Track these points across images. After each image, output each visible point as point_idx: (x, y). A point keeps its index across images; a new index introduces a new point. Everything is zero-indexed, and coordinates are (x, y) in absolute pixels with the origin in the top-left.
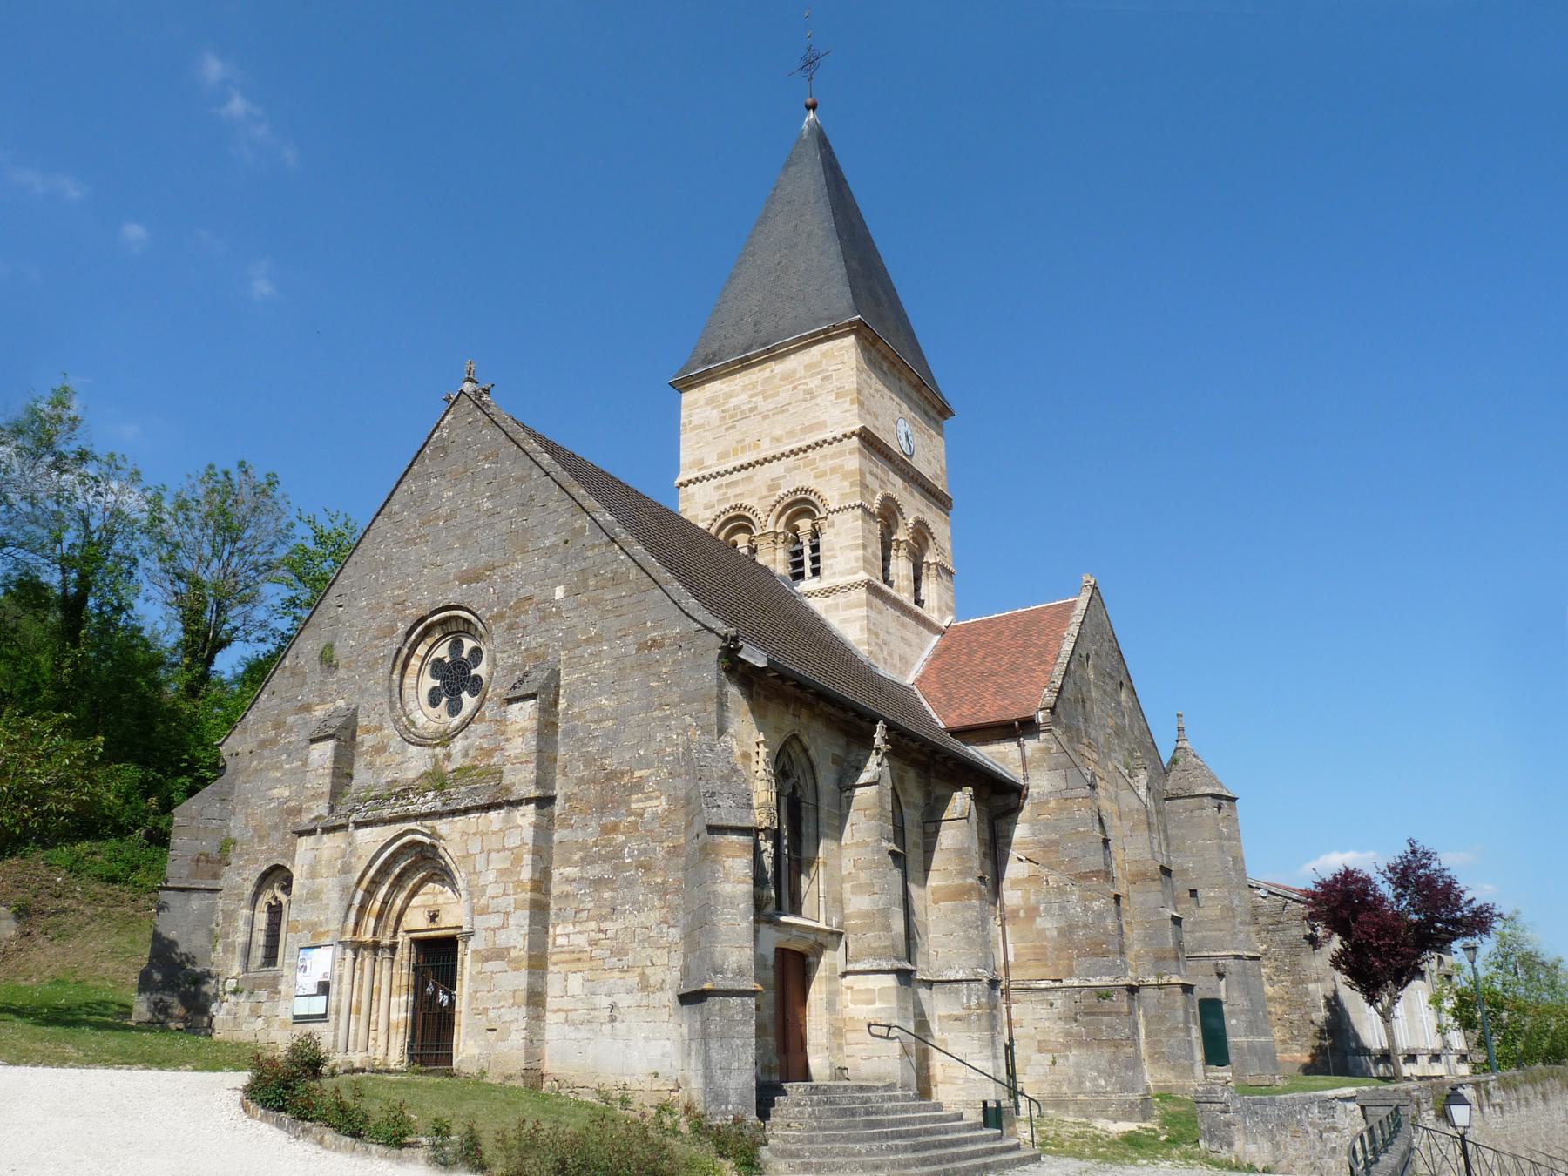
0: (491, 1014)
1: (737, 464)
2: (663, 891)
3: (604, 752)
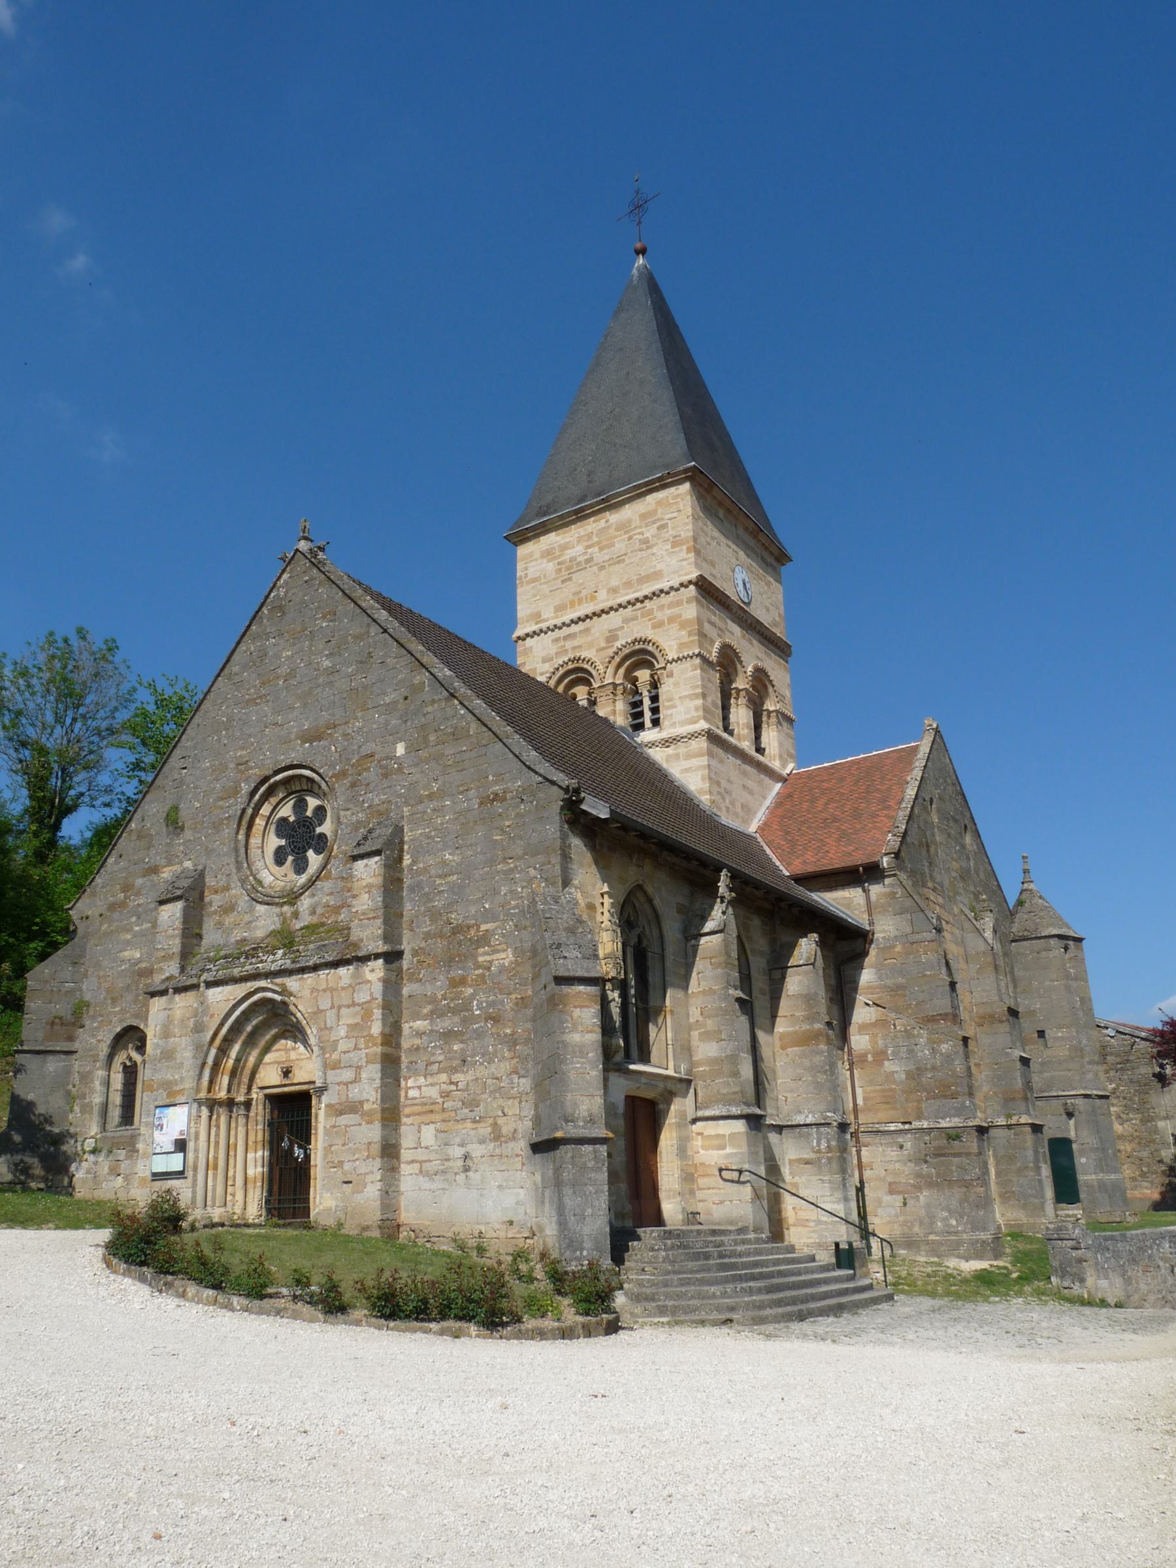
0: (347, 1166)
1: (574, 616)
2: (512, 1042)
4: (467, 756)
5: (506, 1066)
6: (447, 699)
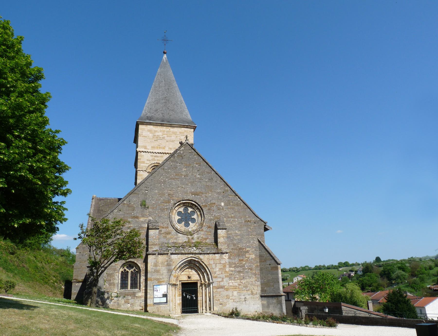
0: (221, 301)
1: (159, 151)
2: (255, 274)
4: (241, 210)
5: (254, 279)
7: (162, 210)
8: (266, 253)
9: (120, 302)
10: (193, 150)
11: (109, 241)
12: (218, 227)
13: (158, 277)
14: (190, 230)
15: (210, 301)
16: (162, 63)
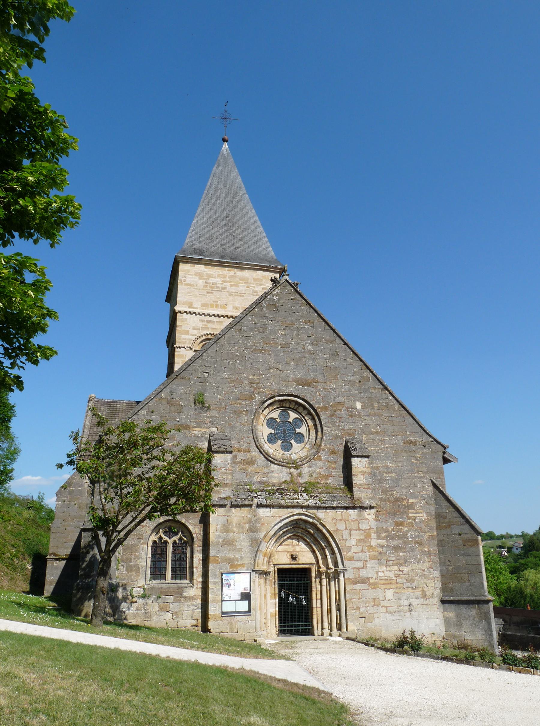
0: (362, 610)
1: (216, 313)
2: (428, 554)
3: (392, 488)
4: (395, 419)
6: (382, 389)
7: (238, 414)
8: (452, 509)
9: (150, 609)
10: (298, 296)
11: (137, 471)
12: (353, 453)
13: (231, 555)
14: (294, 457)
15: (339, 609)
16: (220, 157)
